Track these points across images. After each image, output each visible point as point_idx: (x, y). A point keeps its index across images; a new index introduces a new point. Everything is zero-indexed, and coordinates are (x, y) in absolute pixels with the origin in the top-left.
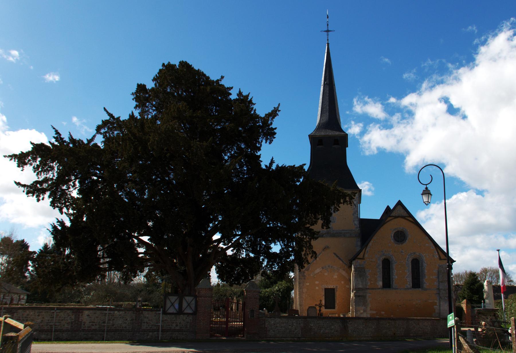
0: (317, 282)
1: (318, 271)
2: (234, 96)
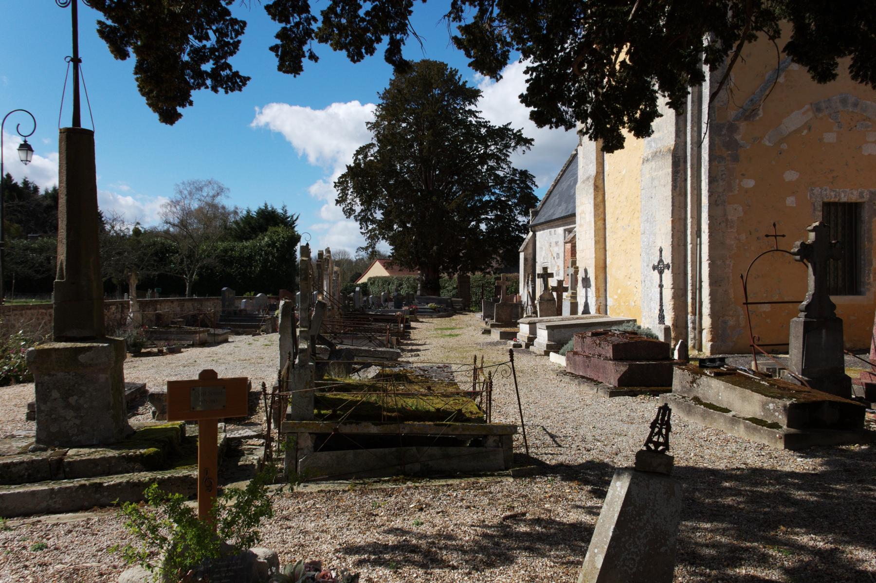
0: (791, 176)
1: (794, 121)
2: (179, 110)
